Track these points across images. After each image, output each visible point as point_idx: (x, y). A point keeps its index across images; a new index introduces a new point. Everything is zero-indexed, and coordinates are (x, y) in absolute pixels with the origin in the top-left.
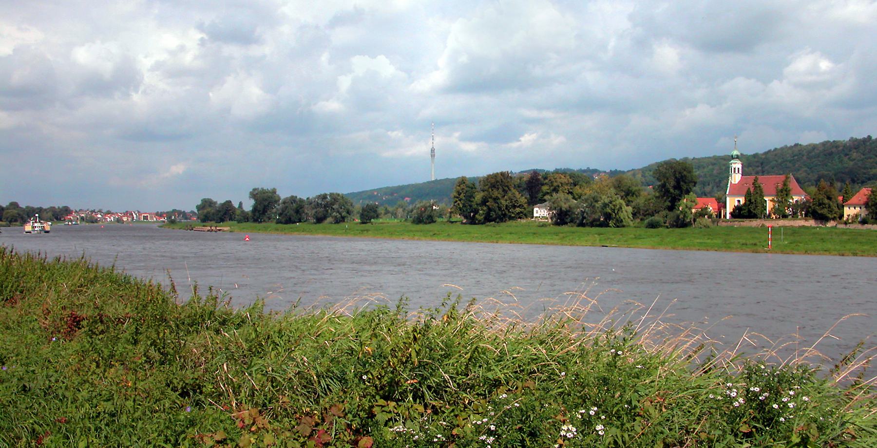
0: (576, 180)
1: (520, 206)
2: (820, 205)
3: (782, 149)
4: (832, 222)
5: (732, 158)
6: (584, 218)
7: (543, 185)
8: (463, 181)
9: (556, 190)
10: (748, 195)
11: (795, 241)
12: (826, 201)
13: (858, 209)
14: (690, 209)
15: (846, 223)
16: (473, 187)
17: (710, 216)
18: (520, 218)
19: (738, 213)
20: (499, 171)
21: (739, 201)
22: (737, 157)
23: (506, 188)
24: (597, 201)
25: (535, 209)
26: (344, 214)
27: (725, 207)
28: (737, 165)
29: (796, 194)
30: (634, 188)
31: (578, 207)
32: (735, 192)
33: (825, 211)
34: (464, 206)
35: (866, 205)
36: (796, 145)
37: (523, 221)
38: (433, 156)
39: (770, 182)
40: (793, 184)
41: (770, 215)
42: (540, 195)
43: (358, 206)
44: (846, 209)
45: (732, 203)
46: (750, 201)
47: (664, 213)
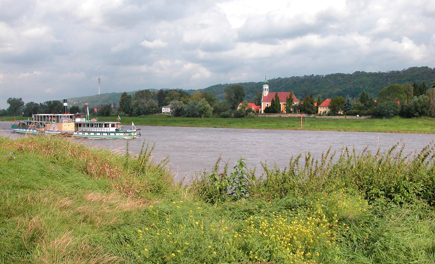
0: (182, 94)
4: (313, 115)
6: (189, 113)
7: (166, 96)
8: (124, 94)
9: (172, 99)
10: (273, 102)
12: (311, 105)
13: (325, 108)
14: (244, 108)
15: (320, 115)
16: (130, 97)
17: (253, 112)
18: (155, 113)
19: (267, 110)
21: (268, 105)
24: (196, 105)
25: (163, 109)
27: (261, 107)
28: (266, 87)
29: (296, 101)
30: (213, 98)
31: (186, 107)
32: (266, 99)
33: (310, 110)
35: (329, 107)
36: (279, 78)
37: (157, 115)
38: (99, 82)
40: (294, 97)
41: (282, 112)
42: (165, 101)
44: (319, 108)
45: (264, 105)
46: (274, 105)
47: (230, 110)
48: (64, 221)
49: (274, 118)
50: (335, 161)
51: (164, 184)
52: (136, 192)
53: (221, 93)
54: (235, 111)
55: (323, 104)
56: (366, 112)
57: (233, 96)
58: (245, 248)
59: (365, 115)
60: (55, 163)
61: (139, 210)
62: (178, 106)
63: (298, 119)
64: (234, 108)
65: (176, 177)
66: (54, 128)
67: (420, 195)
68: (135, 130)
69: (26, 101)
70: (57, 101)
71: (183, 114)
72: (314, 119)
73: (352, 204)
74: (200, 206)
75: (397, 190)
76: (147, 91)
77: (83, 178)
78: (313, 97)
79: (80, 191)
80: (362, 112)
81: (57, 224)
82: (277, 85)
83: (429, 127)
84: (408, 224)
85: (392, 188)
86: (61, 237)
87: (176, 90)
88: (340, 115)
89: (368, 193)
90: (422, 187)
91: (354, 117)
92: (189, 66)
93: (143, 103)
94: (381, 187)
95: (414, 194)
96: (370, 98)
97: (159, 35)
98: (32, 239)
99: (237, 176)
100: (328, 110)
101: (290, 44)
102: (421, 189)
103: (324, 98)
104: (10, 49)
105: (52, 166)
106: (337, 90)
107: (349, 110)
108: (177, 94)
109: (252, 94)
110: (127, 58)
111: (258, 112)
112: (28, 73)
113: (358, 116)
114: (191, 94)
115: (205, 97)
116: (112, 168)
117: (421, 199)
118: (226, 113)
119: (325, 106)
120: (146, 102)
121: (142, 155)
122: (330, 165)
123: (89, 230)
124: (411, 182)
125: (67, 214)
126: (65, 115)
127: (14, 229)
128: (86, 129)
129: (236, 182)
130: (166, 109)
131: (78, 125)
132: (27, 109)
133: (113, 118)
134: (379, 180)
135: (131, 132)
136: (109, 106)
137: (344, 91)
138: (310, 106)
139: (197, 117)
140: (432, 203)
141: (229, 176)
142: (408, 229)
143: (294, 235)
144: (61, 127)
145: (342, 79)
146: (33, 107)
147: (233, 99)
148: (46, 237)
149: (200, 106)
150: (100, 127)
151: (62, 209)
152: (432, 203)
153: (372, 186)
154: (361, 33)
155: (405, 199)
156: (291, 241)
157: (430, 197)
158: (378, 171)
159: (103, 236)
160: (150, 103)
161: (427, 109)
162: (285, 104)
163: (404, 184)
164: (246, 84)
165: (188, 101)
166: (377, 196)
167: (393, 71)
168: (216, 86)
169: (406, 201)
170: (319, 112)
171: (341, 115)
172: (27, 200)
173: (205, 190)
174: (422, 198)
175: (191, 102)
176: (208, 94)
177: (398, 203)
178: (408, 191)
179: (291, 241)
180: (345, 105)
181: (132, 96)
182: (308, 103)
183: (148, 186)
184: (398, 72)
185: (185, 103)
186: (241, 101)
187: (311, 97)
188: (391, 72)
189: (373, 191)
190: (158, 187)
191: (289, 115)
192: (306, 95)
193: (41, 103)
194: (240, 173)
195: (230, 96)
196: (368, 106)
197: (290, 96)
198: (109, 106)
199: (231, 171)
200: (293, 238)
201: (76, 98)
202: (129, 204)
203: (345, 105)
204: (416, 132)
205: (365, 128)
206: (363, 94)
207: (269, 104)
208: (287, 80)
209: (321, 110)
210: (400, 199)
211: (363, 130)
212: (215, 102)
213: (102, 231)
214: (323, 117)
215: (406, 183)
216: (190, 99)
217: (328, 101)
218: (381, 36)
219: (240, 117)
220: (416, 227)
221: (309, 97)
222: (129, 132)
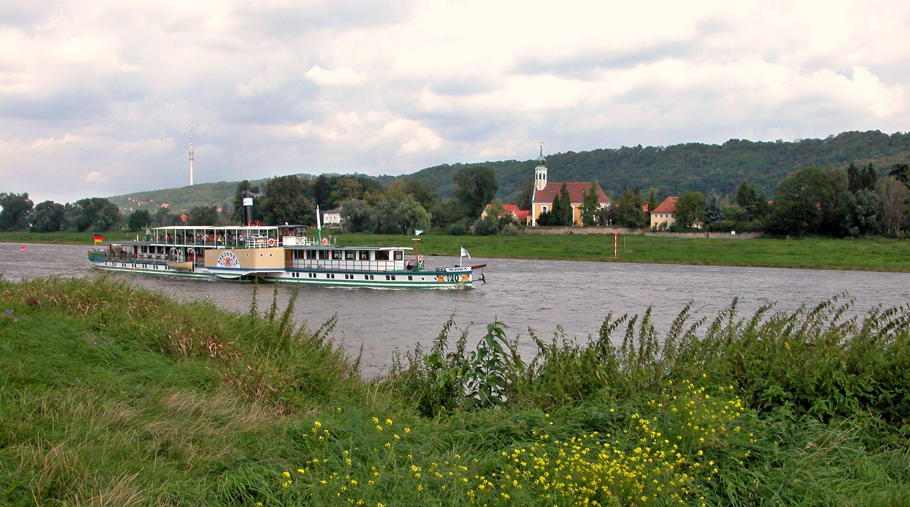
0: (364, 185)
4: (639, 230)
6: (380, 225)
9: (345, 196)
12: (635, 209)
14: (496, 215)
15: (654, 231)
17: (515, 223)
19: (544, 220)
21: (545, 208)
24: (394, 207)
26: (110, 221)
28: (542, 171)
29: (604, 201)
32: (542, 197)
33: (633, 219)
35: (675, 214)
36: (569, 152)
42: (329, 200)
44: (653, 217)
45: (538, 209)
47: (465, 220)
48: (117, 456)
49: (559, 235)
51: (329, 373)
52: (272, 392)
54: (476, 222)
55: (661, 206)
56: (749, 225)
57: (472, 190)
59: (749, 231)
60: (98, 330)
61: (278, 432)
63: (608, 239)
64: (475, 215)
66: (228, 261)
68: (469, 269)
69: (37, 200)
70: (101, 200)
71: (366, 228)
72: (642, 239)
75: (821, 391)
77: (158, 360)
78: (641, 191)
79: (155, 390)
80: (741, 224)
82: (563, 166)
83: (881, 257)
84: (841, 460)
86: (112, 488)
88: (697, 231)
91: (726, 236)
92: (396, 125)
93: (284, 204)
94: (780, 381)
95: (855, 398)
96: (758, 196)
97: (341, 61)
100: (670, 220)
101: (622, 81)
103: (662, 196)
104: (26, 85)
106: (691, 178)
107: (714, 220)
108: (356, 184)
109: (512, 186)
110: (268, 109)
111: (524, 223)
112: (52, 139)
113: (733, 233)
114: (384, 186)
119: (666, 212)
120: (291, 202)
125: (127, 438)
126: (249, 228)
127: (13, 469)
128: (315, 263)
130: (333, 216)
131: (294, 254)
132: (40, 217)
135: (457, 274)
137: (704, 181)
138: (632, 211)
139: (398, 233)
143: (605, 483)
144: (252, 259)
145: (700, 155)
147: (473, 197)
149: (404, 212)
150: (333, 258)
151: (113, 428)
153: (767, 382)
154: (771, 58)
155: (836, 409)
158: (783, 348)
159: (201, 488)
160: (298, 204)
162: (580, 208)
164: (499, 164)
165: (378, 200)
166: (778, 401)
169: (837, 412)
170: (652, 224)
171: (697, 230)
172: (40, 408)
175: (384, 202)
176: (420, 186)
180: (707, 209)
184: (818, 142)
185: (371, 203)
186: (490, 199)
187: (636, 192)
188: (802, 141)
189: (769, 391)
190: (317, 380)
191: (590, 230)
192: (624, 188)
193: (67, 204)
195: (466, 188)
196: (755, 212)
197: (592, 191)
200: (601, 490)
201: (143, 193)
202: (255, 417)
204: (854, 268)
205: (748, 259)
206: (744, 188)
207: (549, 207)
208: (585, 155)
209: (656, 220)
210: (825, 408)
212: (433, 203)
214: (660, 235)
215: (838, 376)
216: (381, 197)
217: (671, 201)
218: (815, 65)
219: (486, 235)
220: (858, 466)
221: (629, 192)
222: (451, 274)
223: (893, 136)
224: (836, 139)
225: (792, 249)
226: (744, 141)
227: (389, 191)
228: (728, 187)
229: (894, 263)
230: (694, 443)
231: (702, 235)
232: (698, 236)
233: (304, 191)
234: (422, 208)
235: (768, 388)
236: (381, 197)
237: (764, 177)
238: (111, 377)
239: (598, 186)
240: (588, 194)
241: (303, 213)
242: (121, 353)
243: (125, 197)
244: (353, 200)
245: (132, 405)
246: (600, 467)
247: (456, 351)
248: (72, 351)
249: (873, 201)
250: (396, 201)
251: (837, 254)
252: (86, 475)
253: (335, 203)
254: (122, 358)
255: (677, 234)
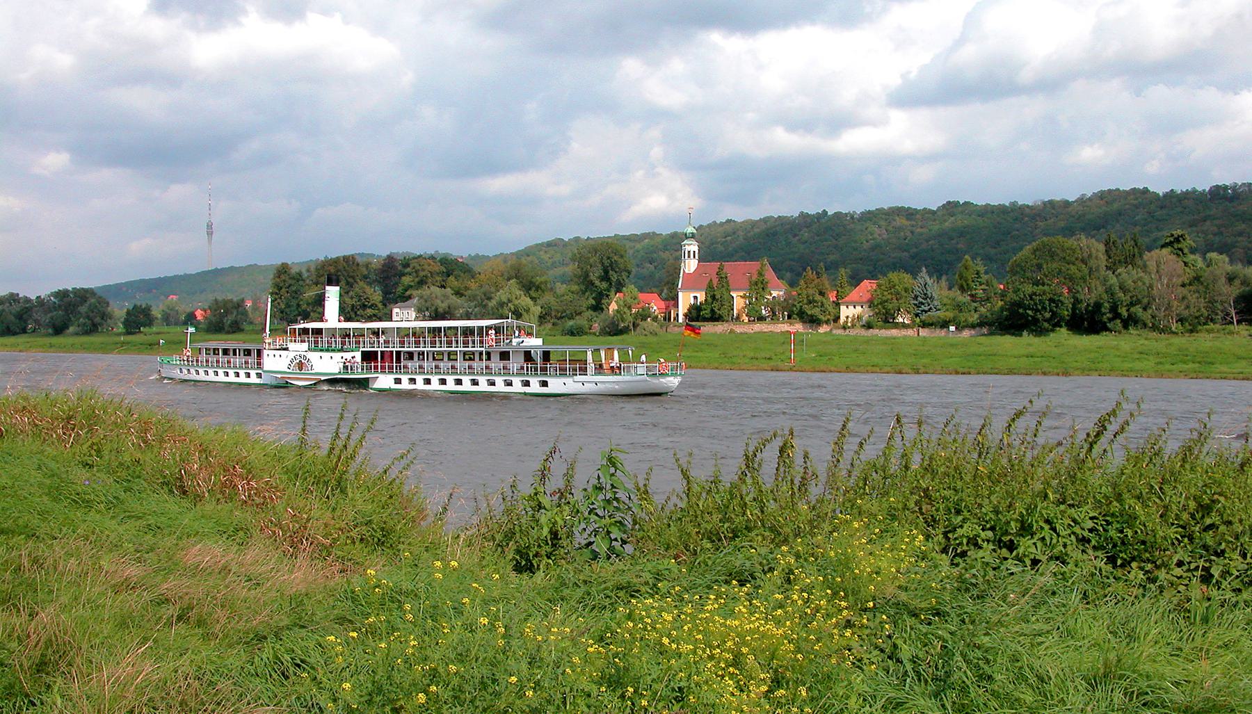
1: (373, 306)
2: (810, 302)
3: (709, 226)
5: (686, 237)
7: (404, 275)
8: (283, 270)
9: (422, 283)
10: (710, 288)
11: (769, 358)
12: (818, 298)
13: (859, 309)
14: (630, 308)
15: (844, 328)
16: (299, 277)
17: (655, 319)
19: (695, 314)
20: (341, 254)
21: (695, 298)
22: (693, 236)
23: (351, 280)
24: (489, 299)
26: (98, 320)
28: (692, 247)
29: (777, 288)
30: (538, 279)
33: (816, 312)
34: (288, 306)
35: (871, 304)
36: (729, 221)
39: (740, 271)
40: (770, 274)
41: (738, 318)
42: (400, 289)
43: (118, 310)
44: (843, 308)
45: (685, 300)
46: (713, 297)
50: (871, 452)
53: (563, 264)
58: (615, 682)
60: (91, 466)
62: (439, 302)
64: (598, 308)
65: (433, 500)
67: (1089, 541)
73: (892, 560)
74: (498, 575)
76: (349, 261)
77: (173, 504)
79: (169, 542)
81: (107, 629)
83: (1151, 358)
84: (1050, 615)
85: (1013, 524)
87: (432, 258)
89: (950, 535)
90: (1091, 518)
94: (979, 517)
98: (42, 666)
99: (601, 497)
102: (1090, 524)
105: (84, 474)
108: (438, 268)
113: (952, 328)
114: (476, 269)
115: (517, 277)
116: (253, 477)
117: (1090, 552)
118: (580, 321)
121: (340, 443)
122: (857, 463)
123: (195, 642)
124: (1062, 507)
125: (133, 601)
129: (598, 511)
133: (254, 336)
134: (979, 501)
136: (239, 305)
137: (913, 257)
140: (1119, 562)
141: (578, 495)
142: (1059, 630)
143: (745, 643)
146: (16, 308)
148: (78, 660)
152: (1119, 562)
153: (960, 518)
156: (737, 662)
157: (1115, 546)
159: (236, 659)
161: (1145, 309)
163: (1044, 512)
166: (974, 542)
167: (1051, 202)
168: (549, 244)
170: (842, 319)
171: (904, 326)
173: (510, 535)
174: (1095, 548)
177: (1028, 562)
178: (1054, 529)
179: (737, 662)
181: (305, 275)
182: (811, 291)
183: (355, 526)
184: (1066, 204)
185: (458, 293)
186: (619, 287)
188: (1044, 203)
190: (383, 529)
191: (758, 327)
194: (609, 487)
198: (239, 305)
199: (584, 477)
203: (916, 298)
205: (971, 364)
209: (847, 312)
210: (1033, 550)
211: (966, 370)
213: (230, 646)
214: (853, 332)
215: (1047, 509)
216: (473, 285)
220: (1071, 622)
223: (1166, 195)
224: (1090, 199)
225: (1031, 350)
226: (966, 203)
227: (482, 276)
228: (945, 267)
229: (1168, 367)
230: (862, 595)
231: (910, 332)
232: (905, 333)
233: (365, 277)
234: (528, 299)
235: (961, 527)
236: (473, 285)
237: (993, 251)
238: (112, 527)
239: (768, 267)
240: (754, 279)
241: (364, 307)
242: (122, 495)
243: (119, 287)
244: (432, 288)
245: (139, 560)
246: (737, 623)
247: (562, 487)
248: (55, 493)
249: (1140, 283)
250: (493, 289)
251: (1092, 355)
252: (85, 646)
253: (408, 293)
254: (122, 502)
255: (876, 331)
